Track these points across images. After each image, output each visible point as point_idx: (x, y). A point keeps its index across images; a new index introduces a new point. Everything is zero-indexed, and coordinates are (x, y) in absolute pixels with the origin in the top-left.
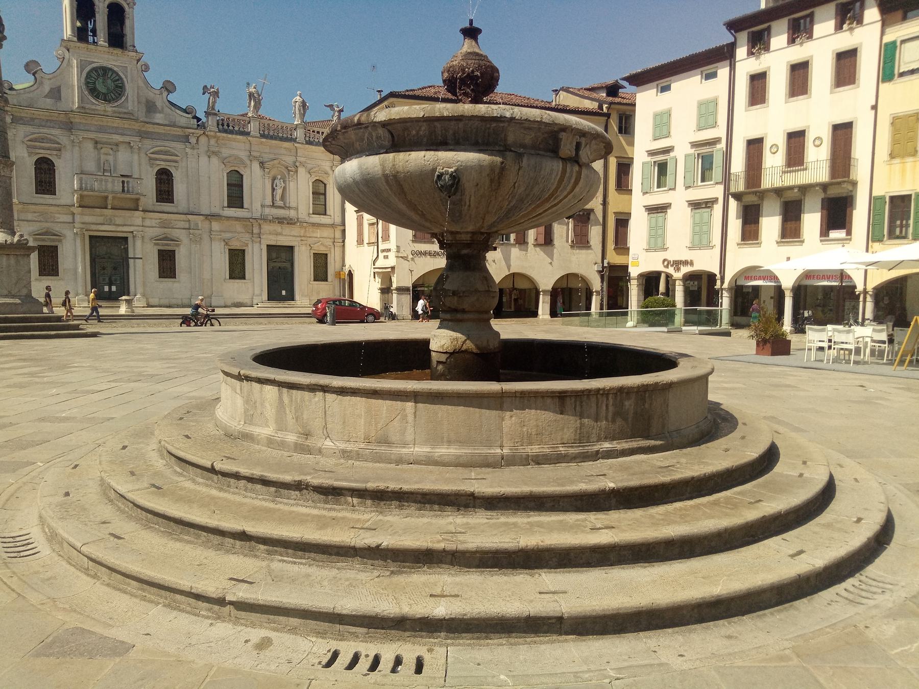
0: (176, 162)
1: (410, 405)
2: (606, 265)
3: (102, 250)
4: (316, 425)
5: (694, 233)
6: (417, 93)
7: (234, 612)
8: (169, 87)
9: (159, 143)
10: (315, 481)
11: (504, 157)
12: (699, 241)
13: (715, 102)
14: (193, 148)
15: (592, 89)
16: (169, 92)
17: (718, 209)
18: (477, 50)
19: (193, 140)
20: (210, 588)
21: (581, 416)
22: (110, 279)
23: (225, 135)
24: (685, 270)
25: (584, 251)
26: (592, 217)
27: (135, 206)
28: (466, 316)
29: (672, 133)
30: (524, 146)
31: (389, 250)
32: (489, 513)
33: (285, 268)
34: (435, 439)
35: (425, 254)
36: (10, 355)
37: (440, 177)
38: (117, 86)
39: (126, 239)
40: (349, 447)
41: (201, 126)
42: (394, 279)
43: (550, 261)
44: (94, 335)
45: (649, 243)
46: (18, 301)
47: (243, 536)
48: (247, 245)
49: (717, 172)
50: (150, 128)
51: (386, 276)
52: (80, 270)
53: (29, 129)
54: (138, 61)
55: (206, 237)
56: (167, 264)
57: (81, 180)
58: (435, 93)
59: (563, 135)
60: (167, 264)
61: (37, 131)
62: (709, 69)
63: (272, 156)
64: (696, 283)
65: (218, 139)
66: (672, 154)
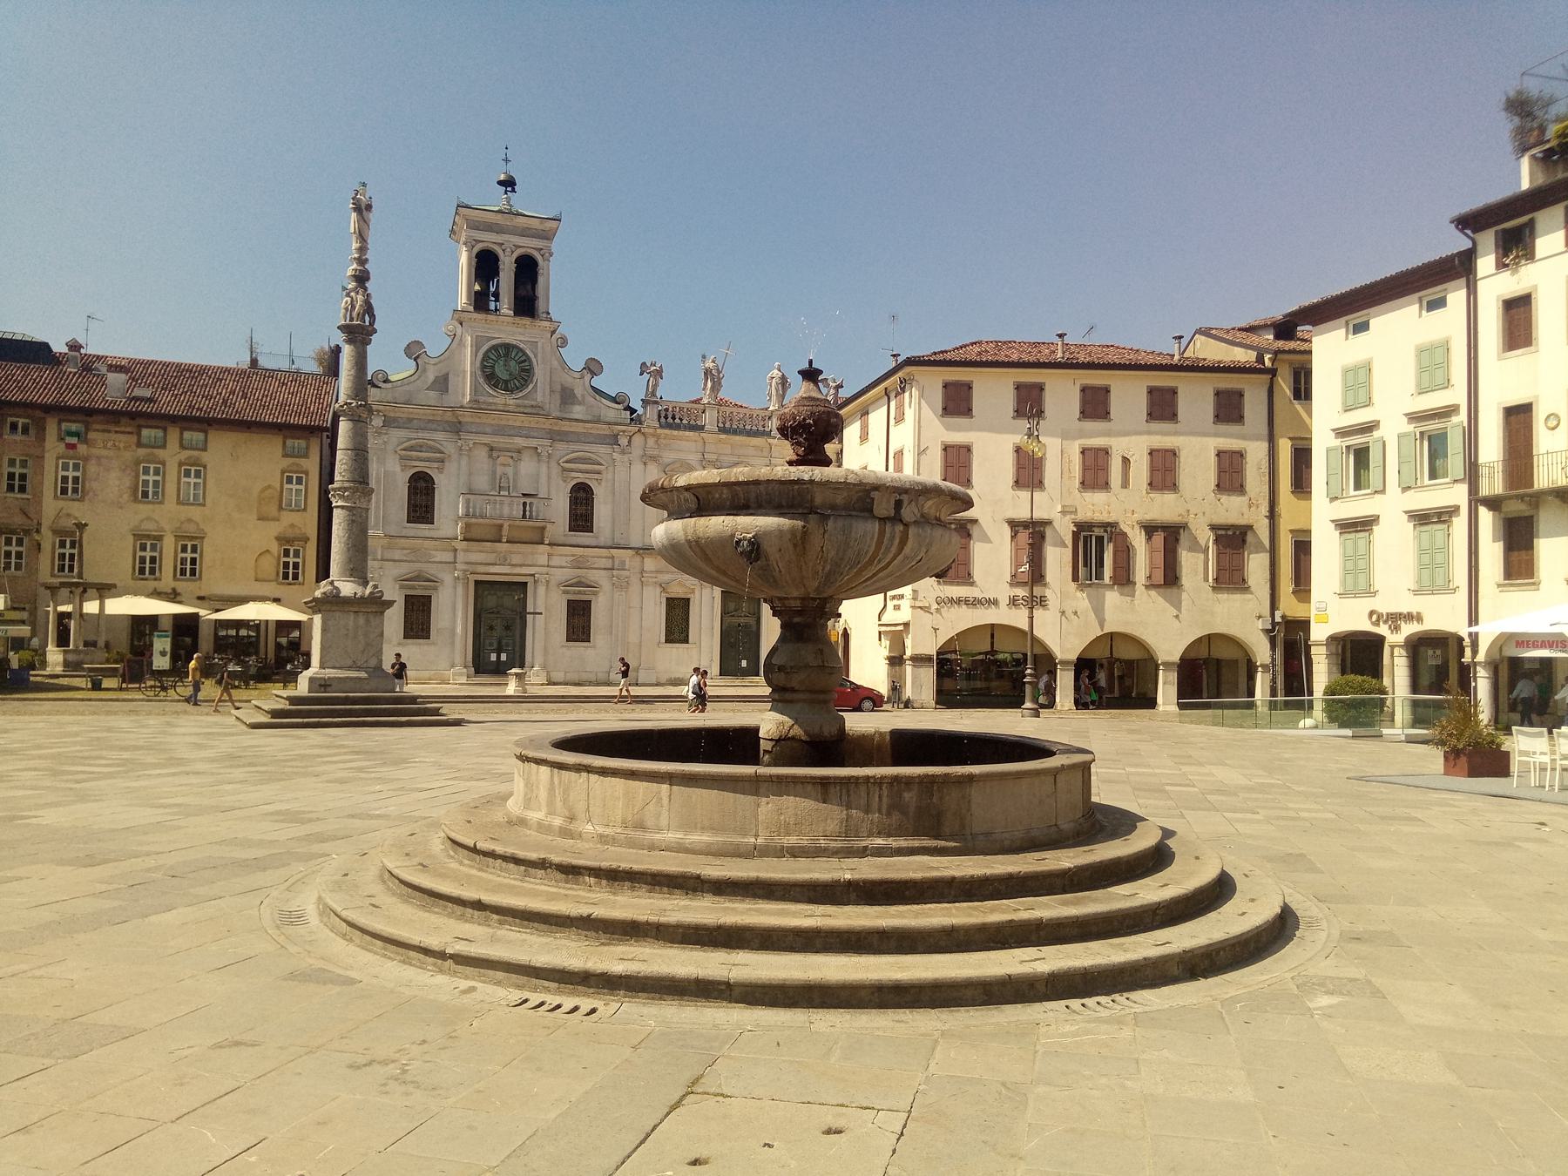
0: (599, 473)
1: (665, 787)
2: (1278, 619)
3: (491, 601)
4: (580, 807)
5: (1421, 567)
6: (948, 356)
7: (453, 966)
8: (593, 367)
9: (573, 446)
10: (556, 859)
11: (806, 521)
12: (1431, 581)
13: (1446, 346)
14: (623, 452)
15: (1251, 329)
16: (594, 374)
17: (1460, 524)
18: (815, 394)
19: (623, 441)
20: (434, 942)
21: (849, 807)
22: (499, 643)
23: (667, 431)
24: (1408, 629)
25: (1237, 596)
26: (1250, 538)
27: (538, 538)
28: (795, 696)
29: (1374, 400)
30: (833, 507)
31: (902, 597)
32: (717, 898)
33: (746, 626)
34: (688, 825)
35: (959, 601)
36: (343, 746)
37: (738, 543)
38: (524, 370)
39: (523, 586)
40: (608, 831)
41: (636, 420)
42: (908, 642)
43: (1175, 612)
44: (457, 723)
45: (1344, 582)
46: (363, 675)
47: (478, 905)
48: (693, 592)
49: (1455, 462)
50: (565, 426)
51: (896, 636)
52: (459, 630)
53: (403, 433)
54: (553, 332)
55: (635, 580)
56: (579, 622)
57: (468, 502)
58: (980, 354)
59: (875, 494)
60: (579, 622)
61: (414, 435)
62: (1432, 293)
63: (735, 459)
64: (1438, 652)
65: (658, 437)
66: (1376, 434)
